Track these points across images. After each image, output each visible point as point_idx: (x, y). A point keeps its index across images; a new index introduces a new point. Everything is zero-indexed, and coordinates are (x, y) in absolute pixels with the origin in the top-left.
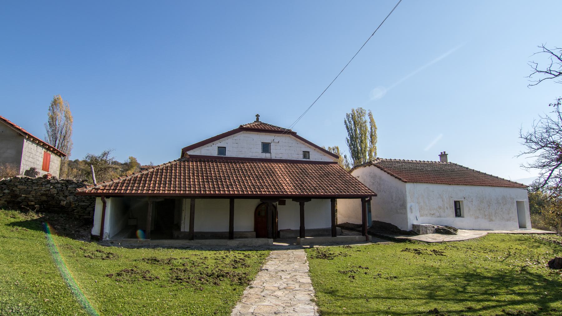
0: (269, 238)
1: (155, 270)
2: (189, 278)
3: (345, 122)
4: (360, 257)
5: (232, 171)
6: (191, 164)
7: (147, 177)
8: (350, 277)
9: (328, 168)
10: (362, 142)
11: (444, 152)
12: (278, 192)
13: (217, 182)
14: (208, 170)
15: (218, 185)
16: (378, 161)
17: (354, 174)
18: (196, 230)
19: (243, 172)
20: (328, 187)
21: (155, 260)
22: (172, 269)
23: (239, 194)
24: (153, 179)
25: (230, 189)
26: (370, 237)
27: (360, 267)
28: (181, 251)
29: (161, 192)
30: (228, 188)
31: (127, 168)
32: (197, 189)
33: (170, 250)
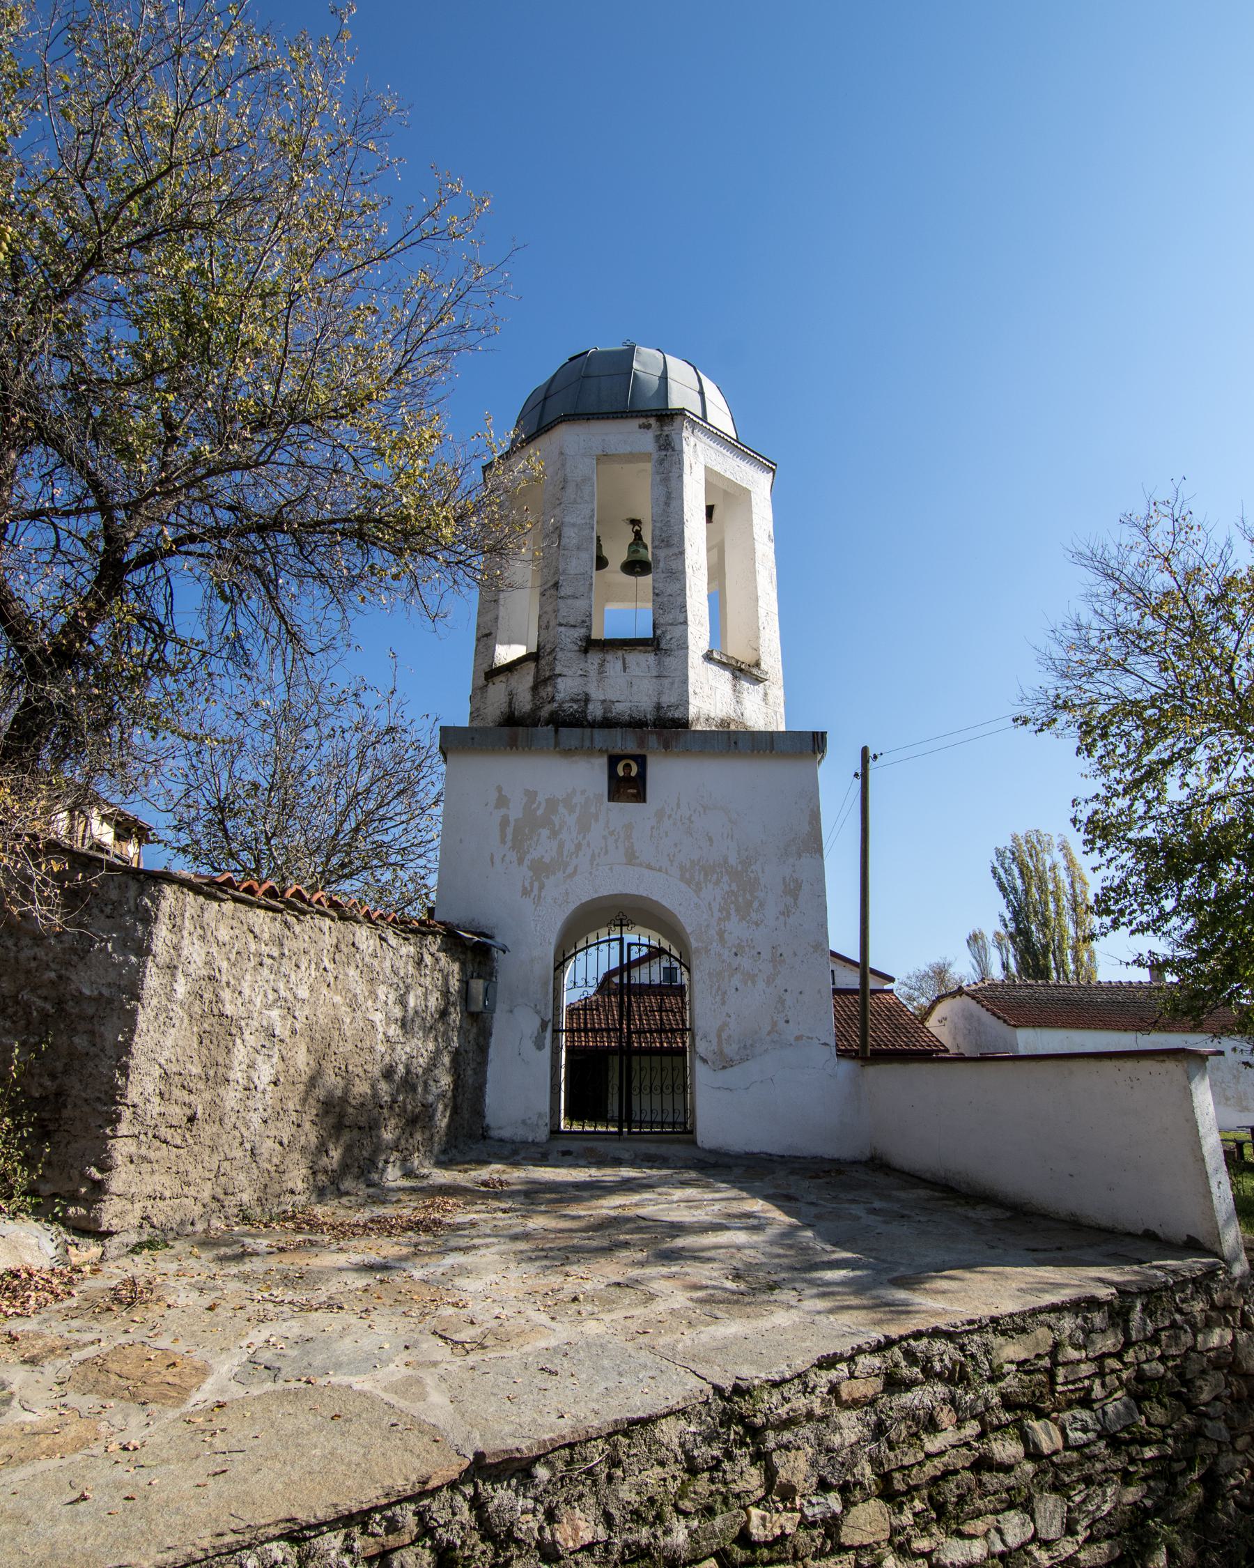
3: (994, 871)
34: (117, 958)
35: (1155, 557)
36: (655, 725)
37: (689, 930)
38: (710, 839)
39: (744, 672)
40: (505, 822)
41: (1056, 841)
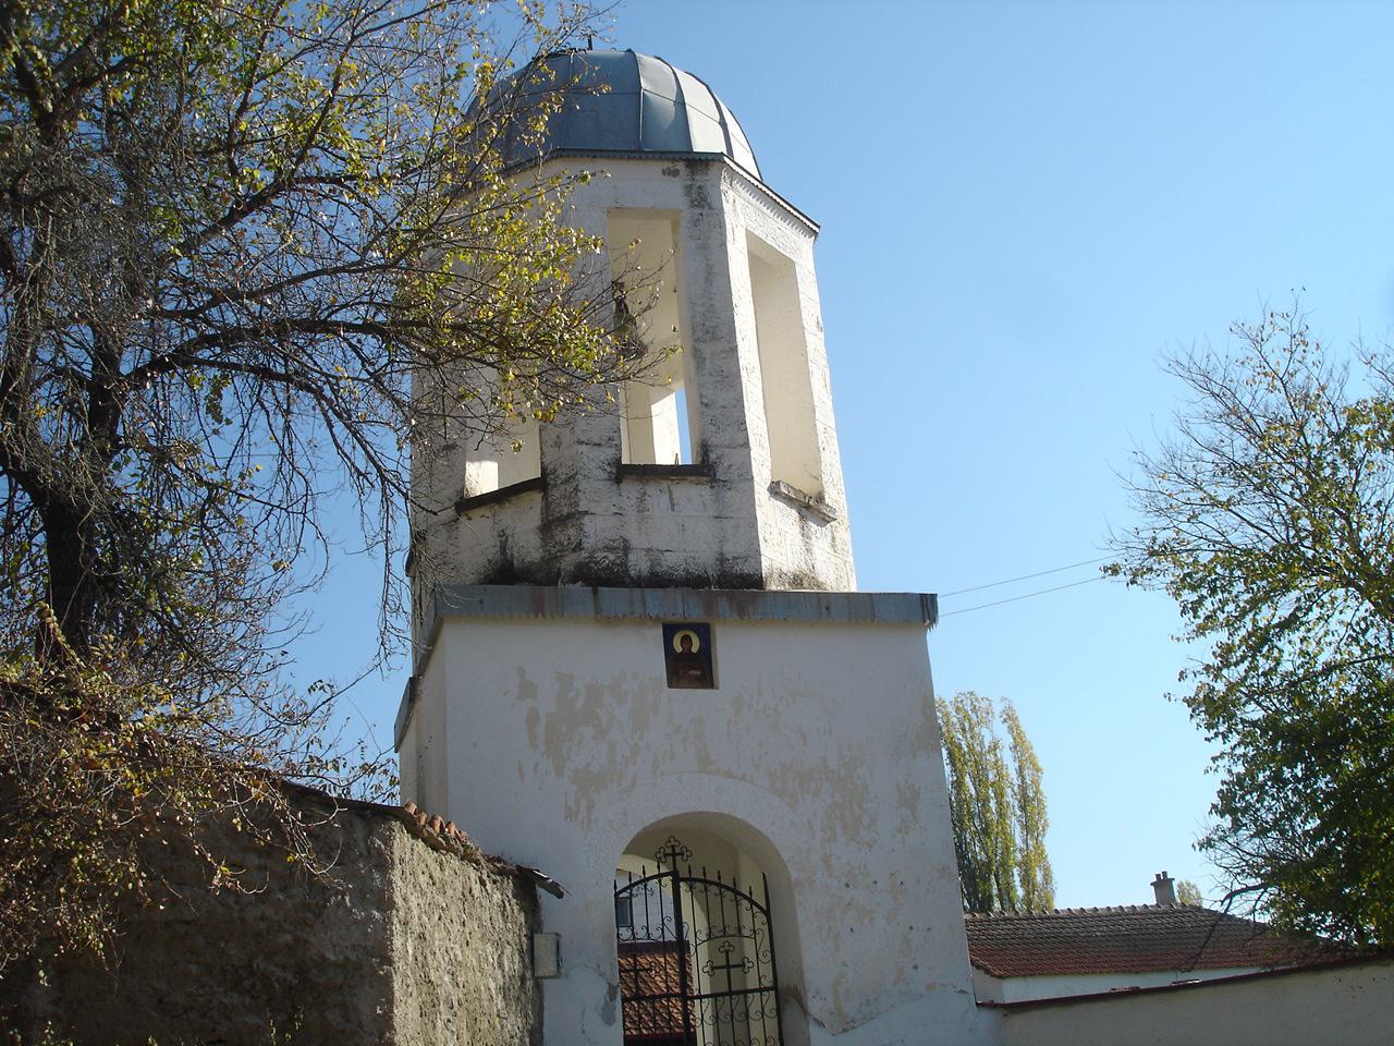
11: (1165, 873)
18: (733, 989)
34: (360, 915)
35: (1266, 374)
36: (719, 584)
37: (785, 856)
38: (804, 736)
39: (810, 508)
40: (533, 719)
41: (998, 708)
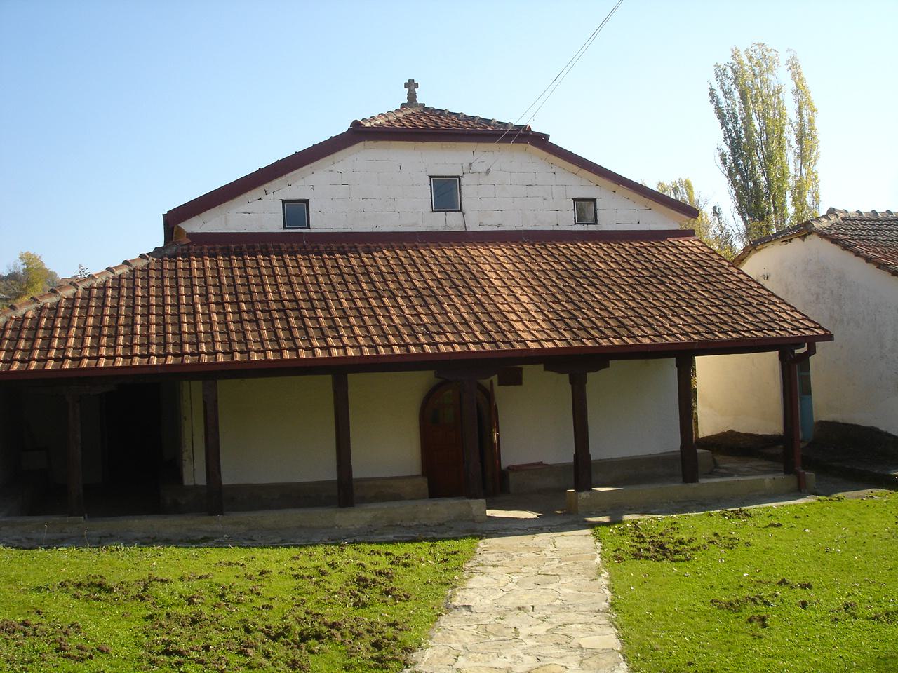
0: (470, 497)
1: (97, 623)
2: (207, 648)
3: (712, 93)
4: (781, 546)
5: (335, 279)
6: (195, 264)
7: (56, 316)
8: (750, 621)
9: (663, 253)
10: (769, 158)
12: (495, 342)
13: (286, 319)
14: (253, 280)
15: (289, 329)
16: (833, 219)
17: (754, 267)
19: (372, 282)
20: (665, 316)
21: (100, 585)
22: (151, 617)
23: (363, 357)
24: (76, 321)
25: (331, 342)
26: (810, 475)
27: (783, 583)
28: (184, 551)
29: (102, 363)
30: (323, 337)
31: (16, 287)
32: (219, 347)
33: (149, 551)
